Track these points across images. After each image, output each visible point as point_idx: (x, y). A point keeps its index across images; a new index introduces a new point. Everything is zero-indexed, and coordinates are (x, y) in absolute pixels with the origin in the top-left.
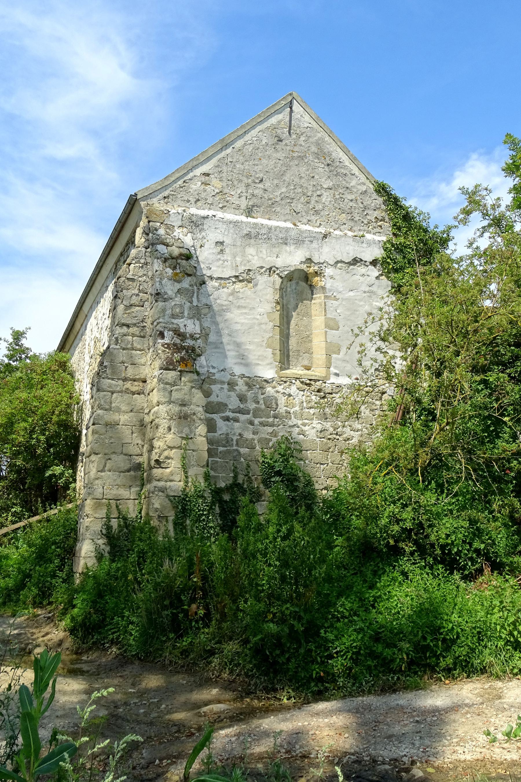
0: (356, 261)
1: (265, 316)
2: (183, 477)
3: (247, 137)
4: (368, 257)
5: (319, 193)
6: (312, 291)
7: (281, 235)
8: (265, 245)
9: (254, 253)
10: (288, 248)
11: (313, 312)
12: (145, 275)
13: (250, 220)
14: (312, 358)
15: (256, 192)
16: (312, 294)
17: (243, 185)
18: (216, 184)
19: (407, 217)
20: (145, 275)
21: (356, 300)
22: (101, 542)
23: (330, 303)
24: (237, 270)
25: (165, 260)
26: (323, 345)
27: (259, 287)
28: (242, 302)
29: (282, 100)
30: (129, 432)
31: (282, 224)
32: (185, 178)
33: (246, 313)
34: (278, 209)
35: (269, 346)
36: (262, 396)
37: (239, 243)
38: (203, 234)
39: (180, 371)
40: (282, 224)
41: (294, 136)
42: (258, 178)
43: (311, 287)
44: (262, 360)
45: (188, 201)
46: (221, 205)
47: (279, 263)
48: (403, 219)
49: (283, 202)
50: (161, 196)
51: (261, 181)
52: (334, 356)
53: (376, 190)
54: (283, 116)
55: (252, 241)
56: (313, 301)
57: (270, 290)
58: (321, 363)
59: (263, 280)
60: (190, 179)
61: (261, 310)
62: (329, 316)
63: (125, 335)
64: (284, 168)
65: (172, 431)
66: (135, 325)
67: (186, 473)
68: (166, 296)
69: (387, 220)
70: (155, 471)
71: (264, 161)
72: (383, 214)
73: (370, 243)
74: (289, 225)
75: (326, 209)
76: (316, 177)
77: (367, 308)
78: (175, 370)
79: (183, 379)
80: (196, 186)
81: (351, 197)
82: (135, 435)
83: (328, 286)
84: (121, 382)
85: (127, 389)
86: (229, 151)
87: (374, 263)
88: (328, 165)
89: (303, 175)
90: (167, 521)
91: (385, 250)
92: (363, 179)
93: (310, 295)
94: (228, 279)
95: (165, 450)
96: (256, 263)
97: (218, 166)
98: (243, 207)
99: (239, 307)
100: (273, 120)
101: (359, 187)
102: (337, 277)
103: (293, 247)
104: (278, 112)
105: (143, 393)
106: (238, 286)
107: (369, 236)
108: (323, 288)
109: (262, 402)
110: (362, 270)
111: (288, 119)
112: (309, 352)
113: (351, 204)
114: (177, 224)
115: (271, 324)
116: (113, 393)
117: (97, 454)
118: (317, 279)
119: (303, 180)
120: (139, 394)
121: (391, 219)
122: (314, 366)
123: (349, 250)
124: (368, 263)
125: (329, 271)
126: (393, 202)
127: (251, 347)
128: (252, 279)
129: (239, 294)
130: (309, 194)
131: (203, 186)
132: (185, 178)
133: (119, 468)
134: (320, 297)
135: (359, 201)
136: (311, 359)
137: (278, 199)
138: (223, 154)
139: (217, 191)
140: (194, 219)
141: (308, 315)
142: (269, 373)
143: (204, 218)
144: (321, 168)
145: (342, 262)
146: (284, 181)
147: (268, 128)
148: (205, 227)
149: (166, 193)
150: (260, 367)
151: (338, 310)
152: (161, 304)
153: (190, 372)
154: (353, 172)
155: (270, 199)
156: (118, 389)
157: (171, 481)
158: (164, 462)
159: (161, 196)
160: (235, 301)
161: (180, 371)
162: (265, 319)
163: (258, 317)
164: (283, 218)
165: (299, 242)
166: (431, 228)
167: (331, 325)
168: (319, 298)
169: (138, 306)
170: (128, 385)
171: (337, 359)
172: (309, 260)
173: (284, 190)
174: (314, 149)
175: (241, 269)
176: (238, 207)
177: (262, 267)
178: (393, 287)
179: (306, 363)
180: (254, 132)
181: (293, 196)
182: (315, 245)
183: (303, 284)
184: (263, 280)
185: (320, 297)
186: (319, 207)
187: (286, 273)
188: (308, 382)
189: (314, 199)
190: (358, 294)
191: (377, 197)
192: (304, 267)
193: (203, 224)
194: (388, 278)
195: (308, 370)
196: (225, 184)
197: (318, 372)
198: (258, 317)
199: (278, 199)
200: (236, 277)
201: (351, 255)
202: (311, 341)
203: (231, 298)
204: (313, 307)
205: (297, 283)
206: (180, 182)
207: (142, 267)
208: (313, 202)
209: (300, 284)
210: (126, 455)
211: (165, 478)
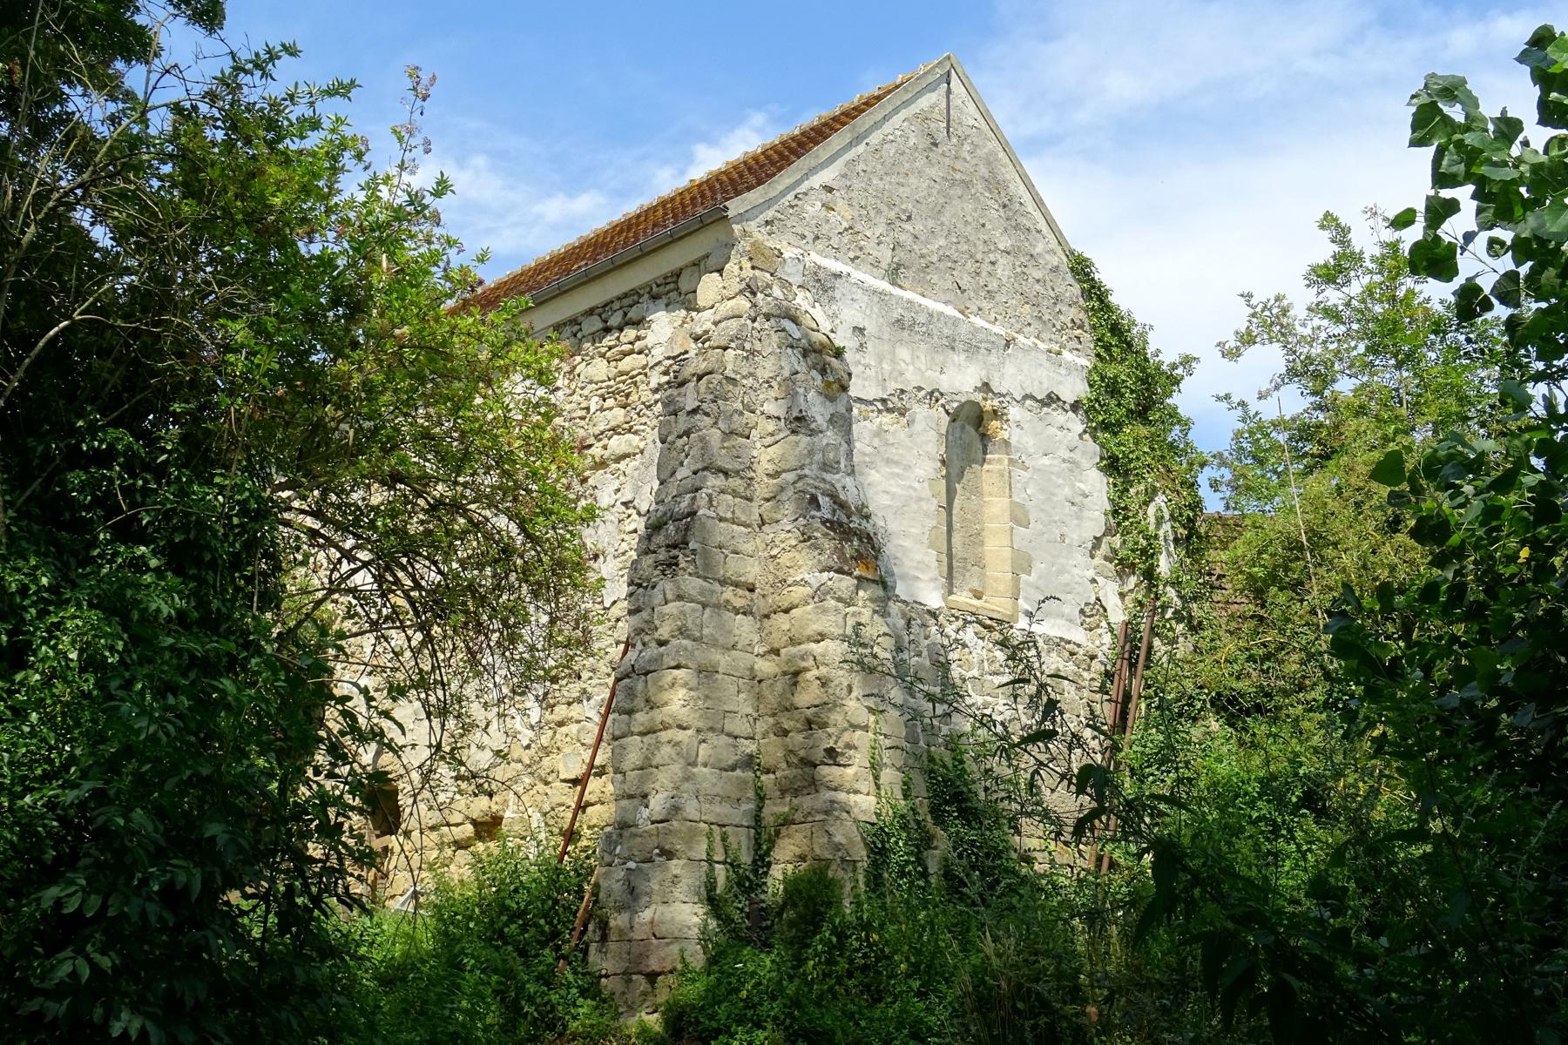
0: (1051, 400)
1: (926, 484)
2: (873, 786)
3: (887, 128)
4: (1069, 396)
5: (992, 257)
6: (985, 448)
7: (946, 331)
8: (922, 345)
9: (908, 359)
10: (956, 358)
11: (986, 488)
12: (751, 374)
13: (896, 291)
14: (984, 575)
15: (903, 238)
16: (985, 453)
17: (883, 220)
18: (843, 214)
19: (1116, 329)
20: (751, 374)
21: (1054, 476)
22: (679, 913)
23: (1018, 472)
24: (884, 389)
25: (805, 354)
26: (1007, 552)
27: (917, 427)
28: (892, 452)
29: (937, 66)
30: (734, 689)
31: (939, 307)
32: (798, 190)
33: (898, 475)
34: (935, 279)
35: (931, 546)
36: (927, 642)
37: (886, 336)
38: (834, 307)
39: (859, 578)
40: (939, 307)
41: (954, 140)
42: (904, 211)
43: (985, 437)
44: (922, 571)
45: (804, 237)
46: (852, 255)
47: (945, 384)
48: (1114, 335)
49: (942, 266)
50: (761, 218)
51: (909, 218)
52: (1023, 577)
53: (1072, 269)
54: (933, 99)
55: (906, 333)
56: (986, 466)
57: (932, 436)
58: (1001, 587)
59: (921, 412)
60: (805, 194)
61: (920, 472)
62: (1015, 498)
63: (722, 492)
64: (942, 200)
65: (854, 694)
66: (737, 472)
67: (876, 778)
68: (813, 426)
69: (1087, 327)
70: (824, 770)
71: (912, 180)
72: (1082, 315)
73: (1071, 368)
74: (950, 311)
75: (1004, 290)
76: (988, 226)
77: (1067, 491)
78: (850, 574)
79: (861, 593)
80: (813, 208)
81: (1038, 274)
82: (742, 696)
83: (1013, 441)
84: (717, 586)
85: (727, 601)
86: (861, 148)
87: (1075, 407)
88: (1005, 206)
89: (970, 219)
90: (855, 870)
91: (1091, 386)
92: (1054, 244)
93: (980, 454)
94: (871, 403)
95: (845, 730)
96: (911, 379)
97: (844, 176)
98: (884, 265)
99: (888, 461)
100: (925, 102)
101: (1047, 256)
102: (1026, 426)
103: (963, 357)
104: (931, 88)
105: (751, 613)
106: (887, 418)
107: (1067, 355)
108: (1006, 443)
109: (925, 653)
110: (1059, 417)
111: (944, 105)
112: (979, 563)
113: (1038, 287)
114: (796, 280)
115: (935, 501)
116: (704, 606)
117: (685, 729)
118: (995, 424)
119: (969, 229)
120: (744, 614)
121: (1094, 327)
122: (988, 592)
123: (1042, 379)
124: (1067, 407)
125: (1014, 412)
126: (1095, 294)
127: (907, 543)
128: (907, 410)
129: (888, 436)
130: (979, 256)
131: (824, 212)
132: (798, 190)
133: (720, 760)
134: (999, 461)
135: (1049, 284)
136: (982, 577)
137: (935, 259)
138: (848, 156)
139: (845, 225)
140: (822, 276)
141: (977, 491)
142: (934, 600)
143: (838, 276)
144: (995, 214)
145: (1032, 397)
146: (942, 224)
147: (916, 116)
148: (837, 294)
149: (770, 214)
150: (921, 585)
151: (1028, 490)
152: (804, 440)
153: (874, 581)
154: (1039, 227)
155: (922, 256)
156: (714, 600)
157: (856, 792)
158: (843, 754)
159: (761, 218)
160: (882, 449)
161: (859, 578)
162: (927, 493)
163: (916, 485)
164: (944, 298)
165: (972, 349)
166: (1150, 350)
167: (1019, 517)
168: (996, 461)
169: (742, 436)
170: (728, 593)
171: (1029, 584)
172: (986, 387)
173: (942, 242)
174: (984, 171)
175: (893, 386)
176: (876, 264)
177: (920, 389)
178: (1102, 458)
179: (976, 585)
180: (897, 120)
181: (954, 257)
182: (993, 359)
183: (971, 430)
184: (921, 412)
185: (999, 461)
186: (993, 285)
187: (955, 405)
188: (988, 622)
189: (986, 267)
190: (1056, 462)
191: (1072, 281)
192: (978, 397)
193: (833, 288)
194: (1095, 438)
195: (979, 598)
196: (856, 214)
197: (996, 605)
198: (916, 485)
199: (935, 259)
200: (884, 401)
201: (1045, 386)
202: (982, 544)
203: (876, 442)
204: (985, 476)
205: (963, 428)
206: (790, 197)
207: (747, 358)
208: (984, 274)
209: (973, 427)
210: (729, 735)
211: (847, 785)
